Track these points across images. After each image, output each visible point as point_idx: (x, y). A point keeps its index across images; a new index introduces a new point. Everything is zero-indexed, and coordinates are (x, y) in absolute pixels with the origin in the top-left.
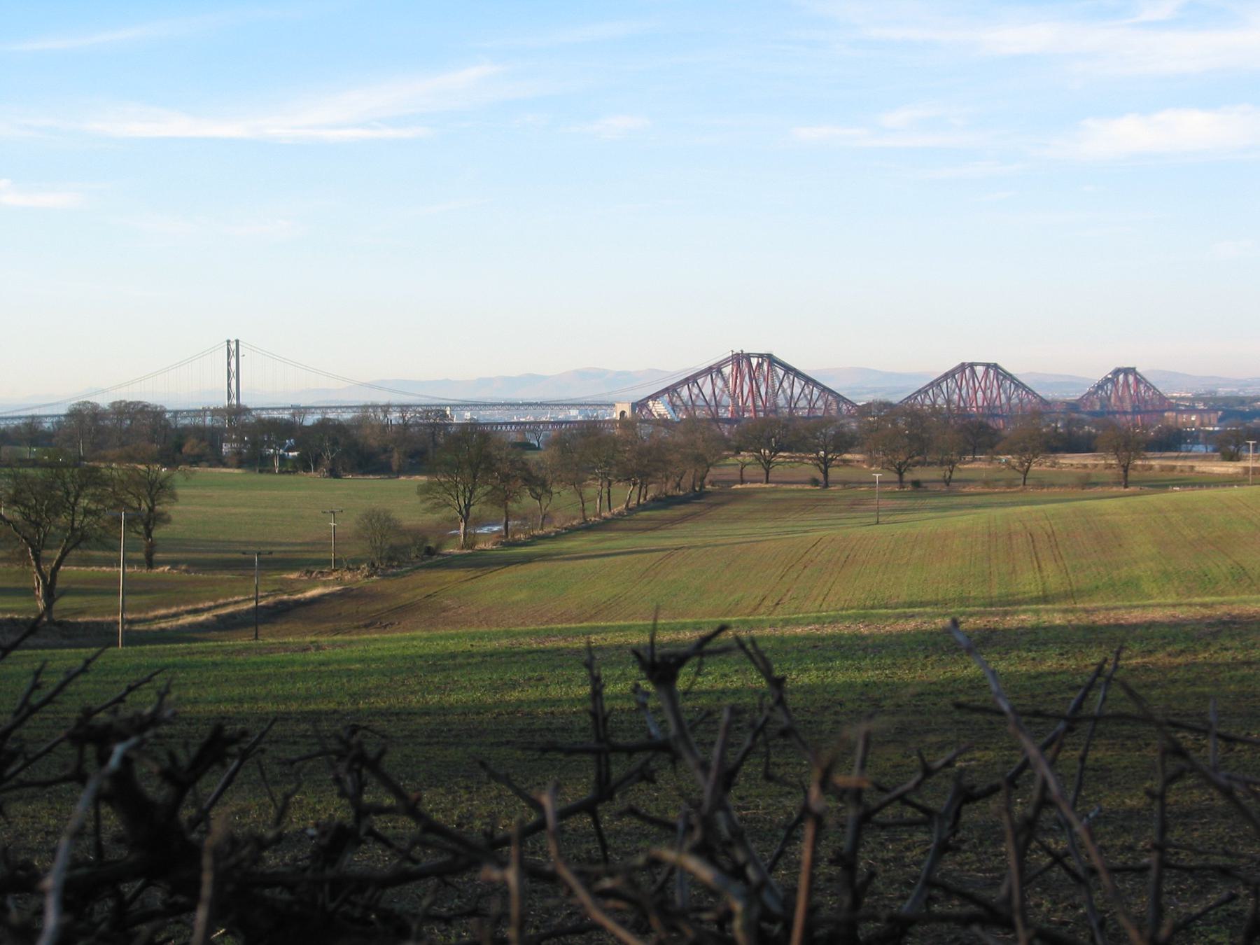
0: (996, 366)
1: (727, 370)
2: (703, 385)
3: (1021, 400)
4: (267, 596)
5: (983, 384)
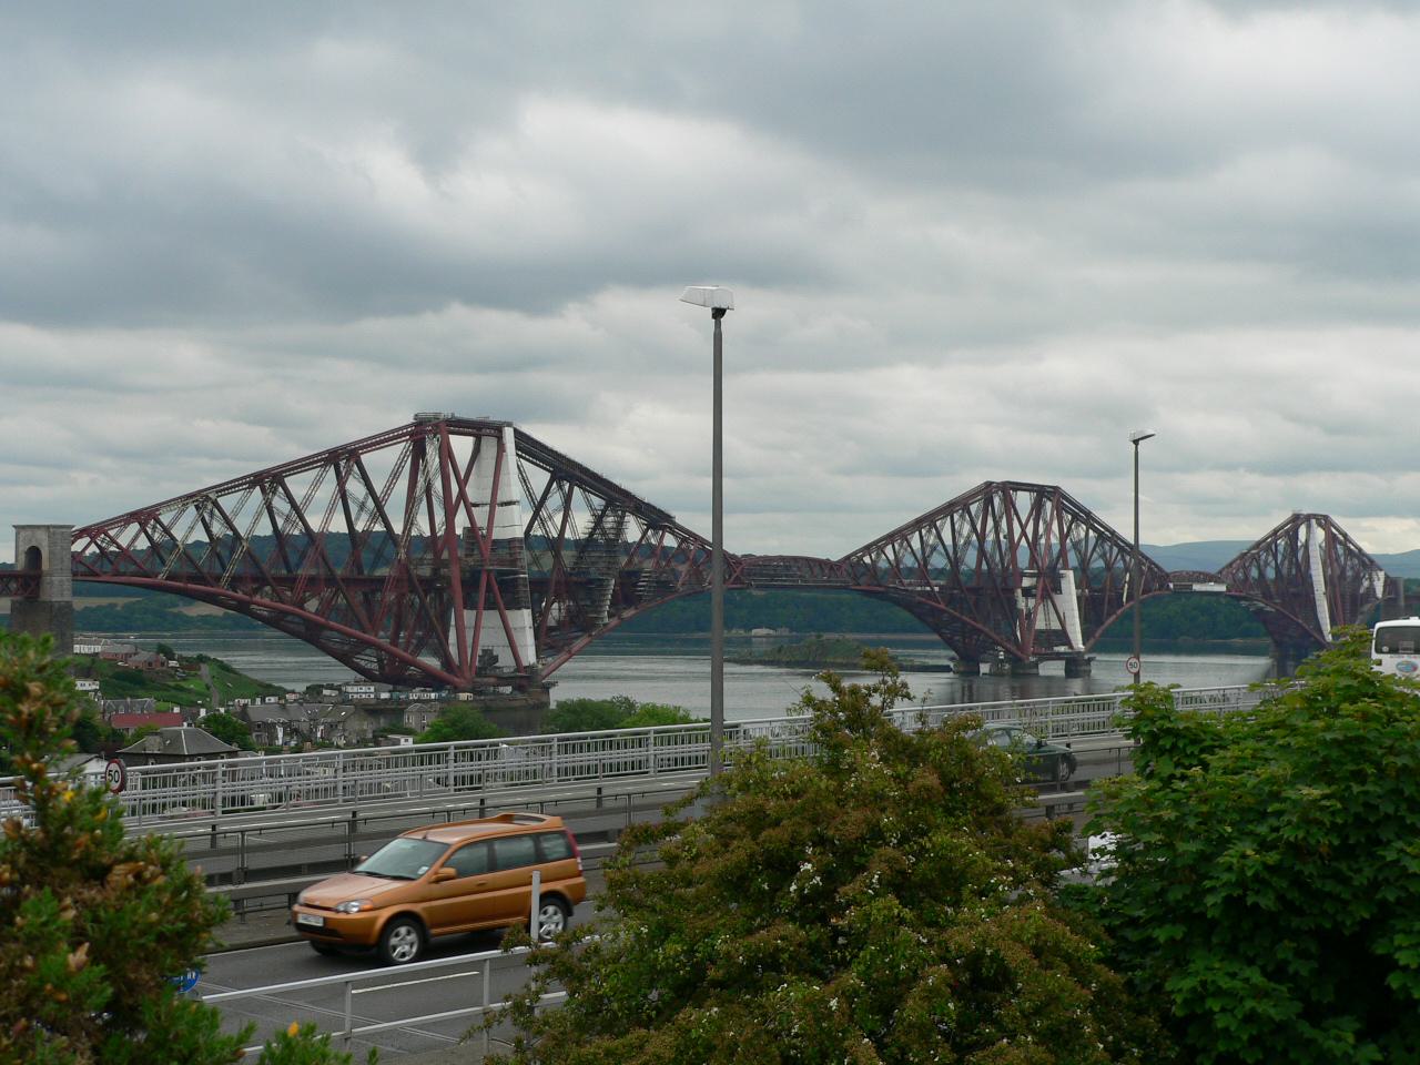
0: (1054, 493)
3: (1109, 567)
4: (1003, 564)
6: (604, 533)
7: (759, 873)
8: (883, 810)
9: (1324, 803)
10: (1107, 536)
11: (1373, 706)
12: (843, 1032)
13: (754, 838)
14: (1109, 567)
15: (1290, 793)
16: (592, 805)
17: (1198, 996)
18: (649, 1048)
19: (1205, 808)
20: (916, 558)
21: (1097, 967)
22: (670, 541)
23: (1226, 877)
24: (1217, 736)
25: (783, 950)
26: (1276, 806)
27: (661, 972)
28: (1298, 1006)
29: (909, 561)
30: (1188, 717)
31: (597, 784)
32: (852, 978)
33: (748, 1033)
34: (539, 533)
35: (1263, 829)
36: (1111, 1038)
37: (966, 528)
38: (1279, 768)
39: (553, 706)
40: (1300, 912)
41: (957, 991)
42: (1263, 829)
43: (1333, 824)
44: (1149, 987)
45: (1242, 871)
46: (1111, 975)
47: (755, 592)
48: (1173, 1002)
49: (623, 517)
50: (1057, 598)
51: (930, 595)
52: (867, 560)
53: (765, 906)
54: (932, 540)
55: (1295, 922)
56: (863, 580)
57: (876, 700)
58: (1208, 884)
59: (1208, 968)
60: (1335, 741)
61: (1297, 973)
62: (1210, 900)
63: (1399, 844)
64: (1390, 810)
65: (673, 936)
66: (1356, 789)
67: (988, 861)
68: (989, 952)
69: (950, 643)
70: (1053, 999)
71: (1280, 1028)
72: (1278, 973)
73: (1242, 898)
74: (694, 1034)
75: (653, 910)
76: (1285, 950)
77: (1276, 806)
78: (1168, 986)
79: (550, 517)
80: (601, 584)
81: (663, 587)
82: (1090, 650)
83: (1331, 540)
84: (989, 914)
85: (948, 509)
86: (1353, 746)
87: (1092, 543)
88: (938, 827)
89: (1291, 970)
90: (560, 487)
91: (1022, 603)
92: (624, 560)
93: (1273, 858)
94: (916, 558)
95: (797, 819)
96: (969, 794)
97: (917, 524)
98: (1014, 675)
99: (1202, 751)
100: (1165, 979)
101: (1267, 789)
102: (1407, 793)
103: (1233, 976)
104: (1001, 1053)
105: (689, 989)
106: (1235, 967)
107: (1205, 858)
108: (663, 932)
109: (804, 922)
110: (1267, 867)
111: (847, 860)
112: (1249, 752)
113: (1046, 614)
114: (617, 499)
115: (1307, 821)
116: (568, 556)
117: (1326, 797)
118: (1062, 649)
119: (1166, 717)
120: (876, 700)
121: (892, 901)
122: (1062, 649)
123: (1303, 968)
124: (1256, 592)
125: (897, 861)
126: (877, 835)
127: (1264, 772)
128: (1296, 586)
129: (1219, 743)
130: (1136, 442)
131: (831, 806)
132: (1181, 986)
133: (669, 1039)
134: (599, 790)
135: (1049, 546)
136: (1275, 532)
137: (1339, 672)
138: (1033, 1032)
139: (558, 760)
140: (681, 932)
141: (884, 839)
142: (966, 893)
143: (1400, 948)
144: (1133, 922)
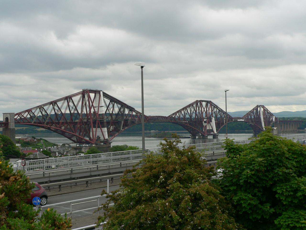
1: (76, 99)
2: (52, 110)
3: (221, 117)
5: (205, 110)
6: (121, 112)
7: (152, 178)
9: (263, 161)
10: (221, 110)
13: (151, 172)
14: (221, 117)
15: (257, 160)
16: (119, 166)
17: (239, 200)
18: (131, 214)
19: (240, 163)
20: (183, 116)
22: (134, 113)
23: (244, 177)
24: (242, 149)
25: (157, 194)
26: (254, 162)
27: (133, 199)
29: (182, 116)
30: (237, 145)
32: (171, 199)
33: (150, 210)
34: (108, 112)
35: (251, 167)
36: (222, 209)
37: (193, 110)
38: (254, 155)
39: (111, 147)
40: (258, 183)
41: (192, 201)
43: (265, 165)
45: (247, 175)
48: (234, 202)
49: (125, 109)
51: (186, 123)
53: (153, 185)
54: (186, 112)
55: (258, 185)
57: (175, 144)
58: (241, 178)
59: (241, 195)
62: (241, 181)
63: (278, 169)
64: (276, 162)
65: (135, 191)
66: (269, 158)
68: (198, 193)
69: (190, 133)
70: (211, 202)
71: (255, 206)
72: (254, 195)
73: (247, 181)
76: (256, 191)
77: (254, 162)
78: (233, 199)
79: (110, 109)
80: (121, 122)
82: (218, 133)
83: (264, 110)
84: (198, 185)
85: (189, 106)
86: (268, 150)
87: (218, 112)
89: (257, 194)
90: (112, 103)
91: (204, 124)
92: (125, 117)
93: (253, 172)
94: (183, 116)
97: (183, 109)
98: (203, 138)
100: (233, 197)
103: (246, 196)
104: (200, 213)
105: (138, 202)
106: (246, 194)
107: (240, 173)
108: (133, 191)
111: (169, 175)
112: (248, 152)
113: (209, 126)
114: (123, 105)
115: (260, 165)
116: (114, 117)
117: (263, 160)
118: (212, 133)
120: (175, 144)
121: (178, 183)
122: (212, 133)
123: (259, 194)
124: (250, 121)
125: (179, 175)
126: (175, 170)
127: (251, 156)
130: (226, 91)
131: (166, 165)
132: (236, 198)
137: (266, 135)
138: (207, 208)
139: (112, 157)
141: (176, 171)
142: (193, 181)
143: (278, 189)
144: (226, 186)
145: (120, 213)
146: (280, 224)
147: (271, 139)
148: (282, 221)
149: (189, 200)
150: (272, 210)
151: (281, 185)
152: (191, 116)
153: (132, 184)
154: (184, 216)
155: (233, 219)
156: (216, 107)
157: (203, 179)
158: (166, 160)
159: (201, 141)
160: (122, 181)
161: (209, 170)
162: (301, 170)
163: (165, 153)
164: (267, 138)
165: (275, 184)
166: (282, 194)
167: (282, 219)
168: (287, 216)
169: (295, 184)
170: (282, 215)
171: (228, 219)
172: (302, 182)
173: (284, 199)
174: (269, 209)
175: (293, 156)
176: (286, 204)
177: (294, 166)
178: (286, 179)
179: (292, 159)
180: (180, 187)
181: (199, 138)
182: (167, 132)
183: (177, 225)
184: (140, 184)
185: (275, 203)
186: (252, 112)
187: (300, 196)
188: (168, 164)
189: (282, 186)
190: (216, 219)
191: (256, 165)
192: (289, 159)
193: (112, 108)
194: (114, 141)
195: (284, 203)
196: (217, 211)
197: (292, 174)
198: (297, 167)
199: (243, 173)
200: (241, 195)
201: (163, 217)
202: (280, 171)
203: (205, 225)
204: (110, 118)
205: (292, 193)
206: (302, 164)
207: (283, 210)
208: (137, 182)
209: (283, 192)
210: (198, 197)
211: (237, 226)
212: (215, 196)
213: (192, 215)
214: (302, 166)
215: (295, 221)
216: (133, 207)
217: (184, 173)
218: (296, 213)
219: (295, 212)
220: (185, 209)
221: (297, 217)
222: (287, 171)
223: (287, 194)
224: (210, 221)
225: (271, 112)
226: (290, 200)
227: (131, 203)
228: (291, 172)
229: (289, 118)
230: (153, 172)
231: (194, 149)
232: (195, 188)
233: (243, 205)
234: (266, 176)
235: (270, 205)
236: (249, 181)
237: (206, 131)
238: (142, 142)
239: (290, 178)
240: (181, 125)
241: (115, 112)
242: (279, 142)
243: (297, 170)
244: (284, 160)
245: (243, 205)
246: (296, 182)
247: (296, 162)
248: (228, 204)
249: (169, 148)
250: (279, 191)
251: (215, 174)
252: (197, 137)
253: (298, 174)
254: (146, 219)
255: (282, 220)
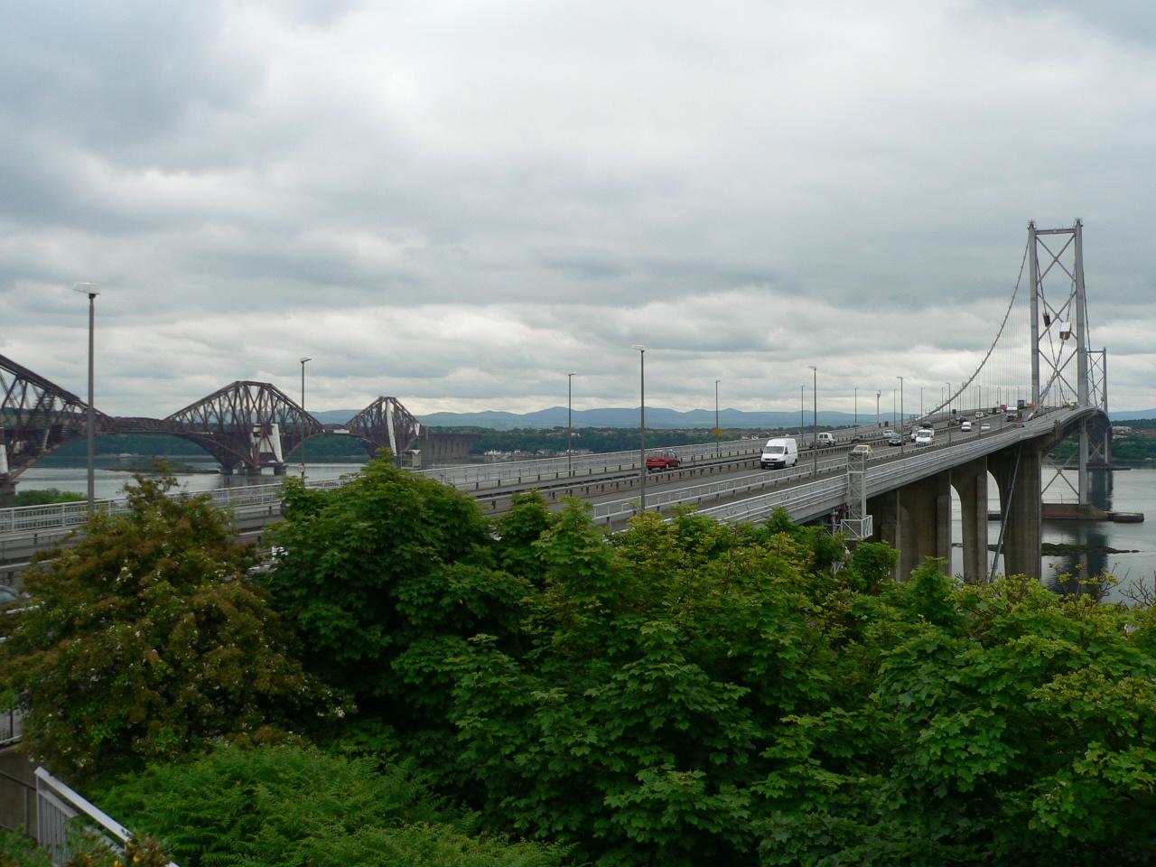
0: (269, 387)
3: (295, 422)
5: (257, 405)
6: (43, 406)
7: (101, 573)
8: (163, 540)
9: (370, 529)
10: (294, 408)
11: (392, 485)
12: (143, 647)
13: (99, 556)
14: (295, 422)
15: (354, 526)
16: (32, 543)
17: (312, 620)
18: (46, 660)
19: (316, 534)
21: (266, 610)
22: (78, 410)
23: (325, 565)
24: (324, 500)
25: (113, 610)
26: (349, 532)
27: (53, 622)
28: (357, 622)
29: (198, 420)
30: (313, 491)
31: (34, 532)
32: (147, 622)
33: (95, 650)
34: (9, 406)
35: (342, 543)
36: (273, 642)
37: (227, 403)
38: (351, 515)
39: (17, 493)
40: (358, 579)
41: (199, 625)
42: (342, 543)
43: (374, 539)
44: (291, 618)
45: (332, 562)
46: (273, 613)
47: (122, 436)
48: (302, 624)
49: (53, 398)
50: (270, 437)
51: (209, 436)
52: (178, 419)
53: (105, 588)
54: (210, 409)
55: (357, 584)
56: (176, 429)
57: (161, 487)
58: (317, 569)
59: (318, 607)
60: (375, 501)
61: (357, 607)
62: (318, 576)
63: (401, 547)
64: (399, 531)
65: (59, 605)
66: (383, 522)
67: (214, 563)
68: (214, 606)
69: (218, 460)
70: (245, 626)
71: (349, 632)
72: (348, 608)
73: (332, 575)
74: (68, 652)
75: (48, 593)
76: (352, 597)
77: (349, 532)
78: (299, 617)
79: (15, 398)
80: (42, 432)
81: (75, 433)
82: (285, 462)
83: (396, 408)
84: (214, 588)
85: (218, 394)
86: (382, 503)
87: (287, 410)
88: (189, 547)
89: (354, 605)
90: (21, 383)
91: (254, 440)
92: (54, 420)
93: (346, 555)
95: (120, 546)
96: (207, 532)
97: (202, 402)
98: (250, 474)
99: (318, 507)
100: (298, 613)
101: (345, 524)
102: (406, 523)
103: (328, 610)
104: (220, 652)
105: (68, 631)
106: (329, 607)
107: (316, 557)
108: (53, 604)
109: (124, 596)
110: (343, 559)
111: (145, 565)
112: (338, 507)
113: (265, 445)
114: (50, 389)
115: (361, 538)
116: (25, 418)
117: (370, 527)
118: (273, 461)
119: (301, 491)
120: (161, 487)
121: (166, 583)
122: (273, 461)
123: (359, 604)
124: (363, 433)
125: (169, 564)
126: (159, 552)
127: (343, 516)
128: (379, 433)
129: (325, 503)
130: (303, 362)
131: (138, 539)
132: (305, 616)
133: (55, 655)
134: (36, 535)
135: (266, 412)
136: (371, 406)
137: (378, 469)
138: (236, 642)
139: (14, 521)
140: (62, 603)
141: (163, 554)
142: (203, 579)
143: (402, 592)
144: (285, 589)
145: (19, 660)
146: (402, 668)
147: (389, 476)
148: (407, 663)
149: (192, 624)
150: (388, 639)
151: (409, 582)
152: (221, 420)
153: (51, 588)
154: (181, 661)
155: (297, 665)
156: (285, 399)
157: (229, 571)
158: (138, 528)
159: (245, 479)
160: (26, 579)
161: (244, 550)
162: (453, 547)
163: (135, 509)
164: (382, 476)
165: (395, 580)
166: (410, 602)
167: (408, 657)
168: (417, 650)
169: (440, 578)
170: (408, 650)
171: (286, 665)
172: (454, 573)
173: (413, 613)
174: (381, 638)
175: (438, 516)
176: (417, 624)
177: (439, 539)
178: (420, 568)
179: (436, 522)
180: (172, 593)
181: (241, 474)
182: (162, 457)
183: (161, 684)
184: (71, 586)
185: (395, 622)
186: (368, 413)
187: (449, 605)
188: (143, 538)
189: (410, 585)
190: (256, 665)
191: (352, 537)
192: (429, 524)
193: (19, 394)
194: (21, 479)
195: (414, 623)
196: (260, 647)
197: (432, 556)
198: (446, 541)
199: (323, 557)
200: (318, 608)
201: (127, 665)
202: (407, 550)
203: (230, 681)
204: (14, 421)
205: (431, 600)
206: (457, 534)
207: (411, 639)
208: (63, 583)
209: (411, 597)
210: (214, 614)
211: (309, 679)
212: (257, 613)
213: (200, 658)
214: (457, 538)
215: (435, 660)
216: (52, 642)
217: (182, 558)
218: (437, 642)
219: (436, 641)
220: (182, 644)
221: (439, 652)
222: (421, 550)
223: (420, 601)
224: (244, 672)
225: (412, 414)
226: (426, 615)
227: (50, 634)
228: (431, 553)
229: (450, 429)
230: (104, 557)
231: (208, 499)
232: (206, 594)
233: (322, 632)
234: (375, 562)
235: (382, 628)
236: (335, 576)
237: (257, 457)
238: (86, 482)
239: (429, 565)
240: (197, 440)
241: (27, 405)
242: (409, 484)
243: (445, 547)
244: (417, 525)
245: (322, 632)
246: (441, 574)
247: (443, 529)
248: (287, 629)
249: (146, 498)
250: (402, 597)
251: (257, 562)
252: (235, 471)
253: (448, 555)
254: (86, 670)
255: (406, 661)
